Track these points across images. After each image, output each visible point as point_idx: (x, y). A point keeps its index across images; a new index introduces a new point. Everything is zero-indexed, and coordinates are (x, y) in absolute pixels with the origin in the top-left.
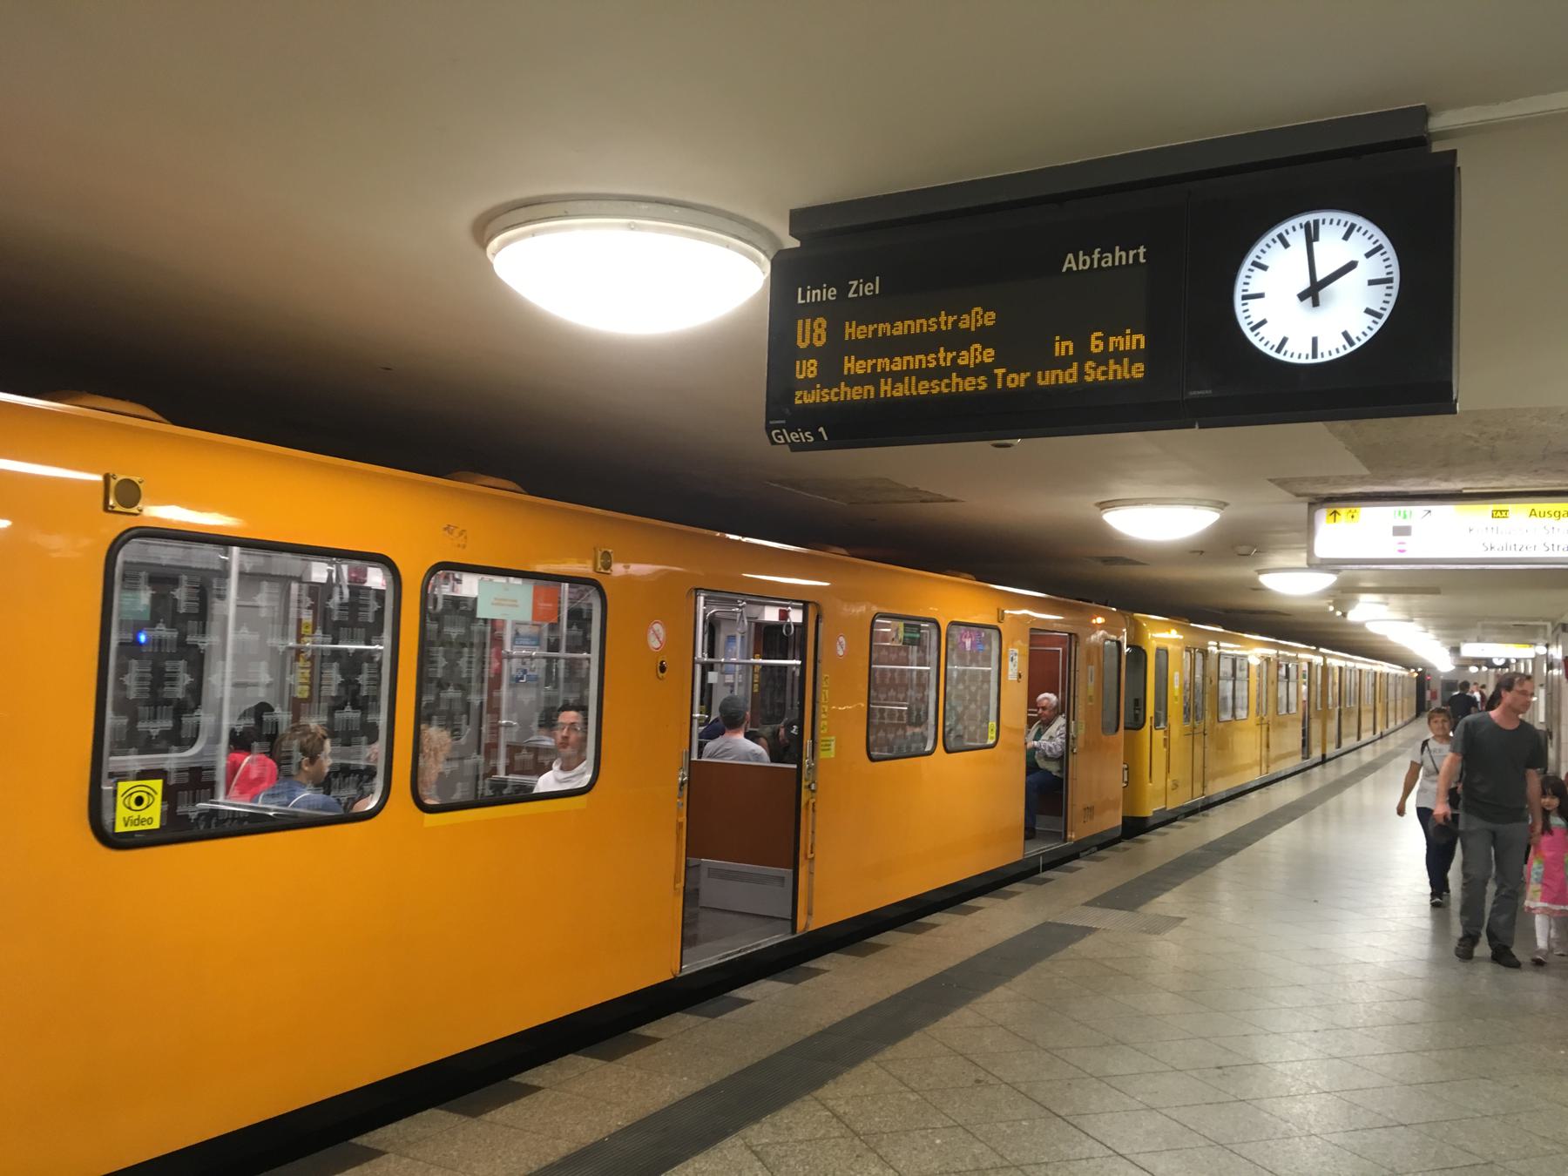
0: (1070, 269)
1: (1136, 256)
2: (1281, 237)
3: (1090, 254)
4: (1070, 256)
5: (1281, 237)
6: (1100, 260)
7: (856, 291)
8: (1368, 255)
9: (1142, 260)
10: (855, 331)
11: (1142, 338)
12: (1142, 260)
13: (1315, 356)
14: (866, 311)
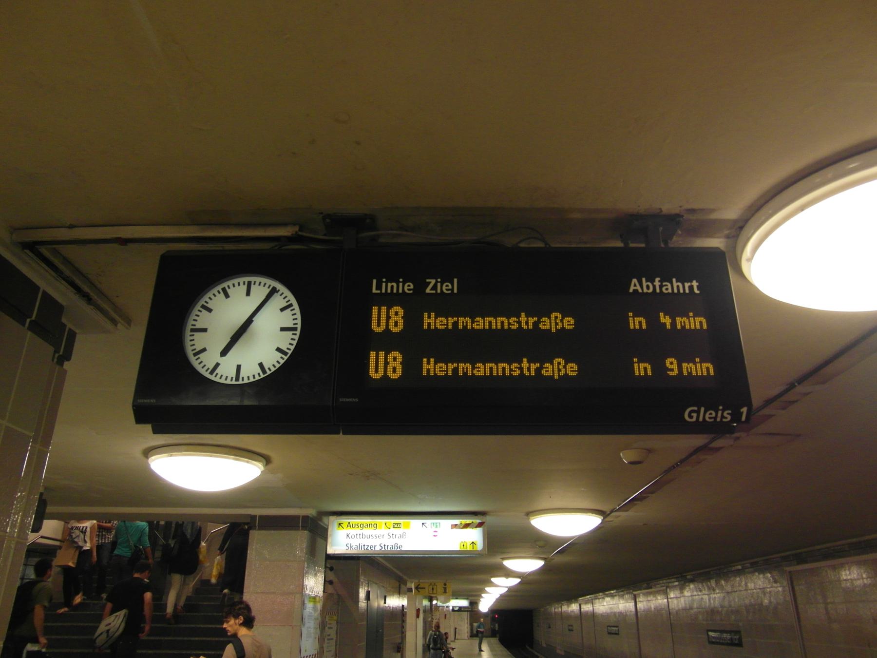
0: (635, 291)
1: (691, 288)
2: (224, 290)
3: (653, 281)
4: (635, 281)
5: (224, 290)
6: (661, 287)
7: (434, 287)
8: (217, 365)
10: (432, 321)
11: (704, 321)
14: (443, 305)
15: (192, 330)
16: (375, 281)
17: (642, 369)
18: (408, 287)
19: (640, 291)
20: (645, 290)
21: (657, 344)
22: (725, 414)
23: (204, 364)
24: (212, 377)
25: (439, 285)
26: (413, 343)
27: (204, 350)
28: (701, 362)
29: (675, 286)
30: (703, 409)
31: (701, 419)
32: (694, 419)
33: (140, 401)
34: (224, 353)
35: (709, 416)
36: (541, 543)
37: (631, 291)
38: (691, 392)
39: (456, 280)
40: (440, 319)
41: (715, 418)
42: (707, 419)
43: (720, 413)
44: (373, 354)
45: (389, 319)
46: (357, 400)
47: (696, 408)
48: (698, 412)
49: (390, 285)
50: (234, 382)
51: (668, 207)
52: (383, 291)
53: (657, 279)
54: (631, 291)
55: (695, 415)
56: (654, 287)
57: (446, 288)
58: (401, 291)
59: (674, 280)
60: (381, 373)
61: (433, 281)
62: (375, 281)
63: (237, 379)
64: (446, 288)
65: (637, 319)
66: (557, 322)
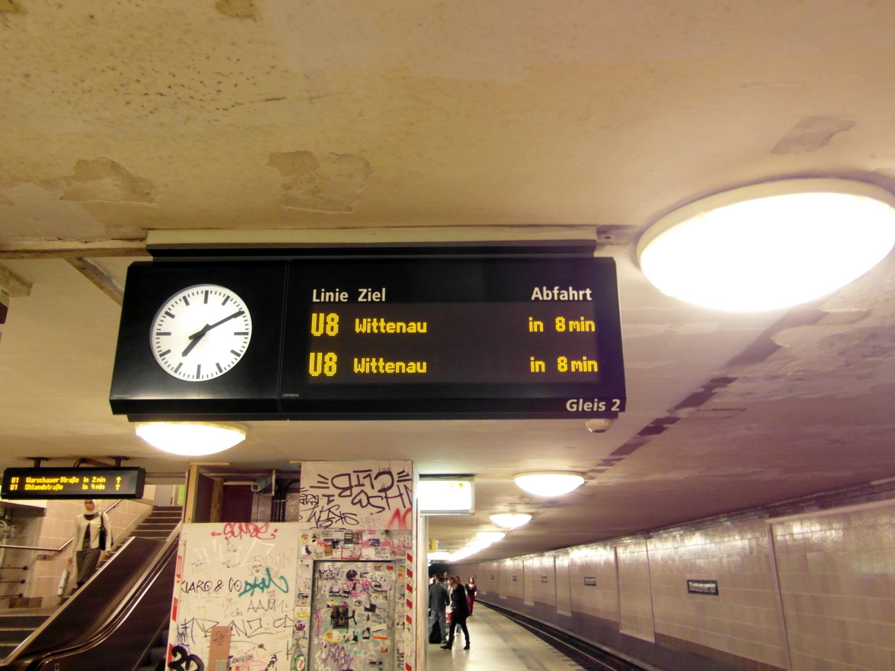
0: (537, 299)
1: (585, 295)
2: (185, 298)
3: (552, 289)
4: (537, 289)
5: (185, 298)
6: (559, 294)
7: (366, 296)
8: (181, 364)
9: (589, 298)
12: (589, 298)
13: (198, 377)
14: (372, 310)
15: (158, 334)
16: (315, 291)
17: (537, 366)
18: (344, 296)
19: (541, 298)
20: (545, 298)
21: (552, 345)
22: (600, 405)
23: (169, 364)
24: (176, 375)
25: (370, 294)
26: (348, 345)
27: (169, 351)
28: (587, 360)
29: (571, 294)
30: (581, 401)
31: (580, 409)
32: (575, 409)
33: (116, 397)
34: (185, 353)
35: (587, 406)
36: (527, 500)
37: (533, 298)
38: (582, 387)
39: (384, 290)
40: (389, 324)
41: (593, 408)
42: (585, 409)
43: (596, 404)
44: (312, 355)
45: (324, 324)
46: (297, 395)
47: (575, 401)
48: (578, 403)
49: (328, 294)
50: (195, 380)
51: (624, 223)
52: (322, 300)
53: (556, 288)
54: (533, 298)
55: (575, 406)
56: (553, 294)
57: (375, 296)
58: (337, 300)
59: (571, 288)
60: (319, 371)
61: (365, 291)
62: (315, 291)
63: (198, 377)
64: (375, 296)
65: (536, 323)
66: (417, 328)
